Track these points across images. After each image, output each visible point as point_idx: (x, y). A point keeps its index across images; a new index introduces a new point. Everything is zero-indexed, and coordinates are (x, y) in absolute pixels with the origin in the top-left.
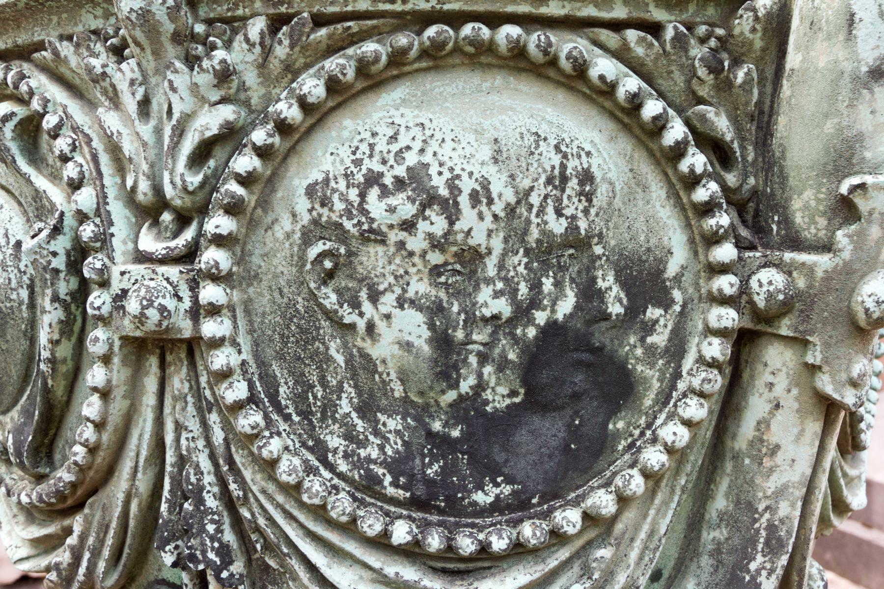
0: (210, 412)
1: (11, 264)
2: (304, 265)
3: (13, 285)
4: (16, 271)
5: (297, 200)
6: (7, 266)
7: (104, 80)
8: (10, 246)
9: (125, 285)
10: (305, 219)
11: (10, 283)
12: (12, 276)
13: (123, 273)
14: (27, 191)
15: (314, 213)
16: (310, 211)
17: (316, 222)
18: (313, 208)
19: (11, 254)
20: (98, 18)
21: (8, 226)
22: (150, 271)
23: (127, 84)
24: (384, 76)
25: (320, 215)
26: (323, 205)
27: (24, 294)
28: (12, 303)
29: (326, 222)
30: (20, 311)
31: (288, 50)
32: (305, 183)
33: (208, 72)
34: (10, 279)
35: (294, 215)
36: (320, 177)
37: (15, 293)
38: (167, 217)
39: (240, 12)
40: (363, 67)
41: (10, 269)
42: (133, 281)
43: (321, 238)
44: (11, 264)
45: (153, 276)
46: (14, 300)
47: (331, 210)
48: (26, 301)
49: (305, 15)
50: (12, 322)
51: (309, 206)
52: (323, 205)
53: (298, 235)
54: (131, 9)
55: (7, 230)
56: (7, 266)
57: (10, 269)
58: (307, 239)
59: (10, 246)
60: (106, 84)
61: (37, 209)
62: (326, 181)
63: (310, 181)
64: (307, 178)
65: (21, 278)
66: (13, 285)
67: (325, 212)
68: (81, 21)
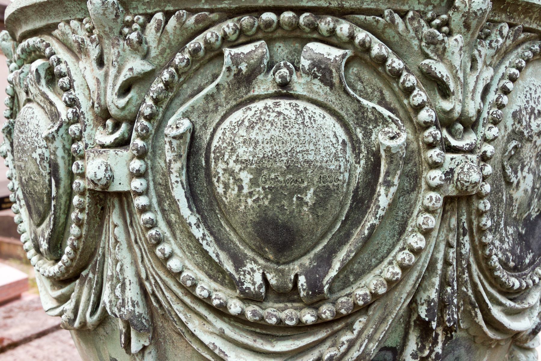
0: (464, 235)
1: (342, 155)
2: (505, 153)
3: (342, 170)
4: (344, 160)
5: (508, 120)
6: (339, 157)
7: (441, 44)
8: (340, 143)
9: (452, 166)
10: (510, 129)
11: (340, 169)
12: (342, 164)
13: (452, 159)
14: (351, 107)
15: (514, 127)
16: (513, 125)
17: (513, 131)
18: (514, 124)
19: (341, 149)
20: (421, 4)
21: (334, 129)
22: (464, 157)
23: (458, 49)
24: (254, 37)
25: (516, 128)
26: (519, 122)
27: (347, 175)
28: (339, 182)
29: (518, 131)
30: (343, 187)
31: (511, 42)
32: (512, 111)
33: (495, 49)
34: (340, 166)
35: (506, 127)
36: (518, 109)
37: (342, 175)
38: (109, 122)
39: (496, 18)
40: (241, 32)
41: (340, 159)
42: (456, 163)
43: (514, 139)
44: (342, 155)
45: (467, 160)
46: (340, 180)
47: (521, 125)
48: (347, 181)
49: (521, 26)
50: (335, 195)
51: (513, 123)
52: (519, 122)
53: (506, 138)
54: (481, 8)
55: (335, 132)
56: (339, 157)
57: (340, 159)
58: (510, 139)
59: (340, 143)
60: (440, 47)
61: (357, 119)
62: (520, 110)
63: (513, 110)
64: (512, 109)
65: (347, 165)
66: (342, 170)
67: (518, 126)
68: (408, 3)
